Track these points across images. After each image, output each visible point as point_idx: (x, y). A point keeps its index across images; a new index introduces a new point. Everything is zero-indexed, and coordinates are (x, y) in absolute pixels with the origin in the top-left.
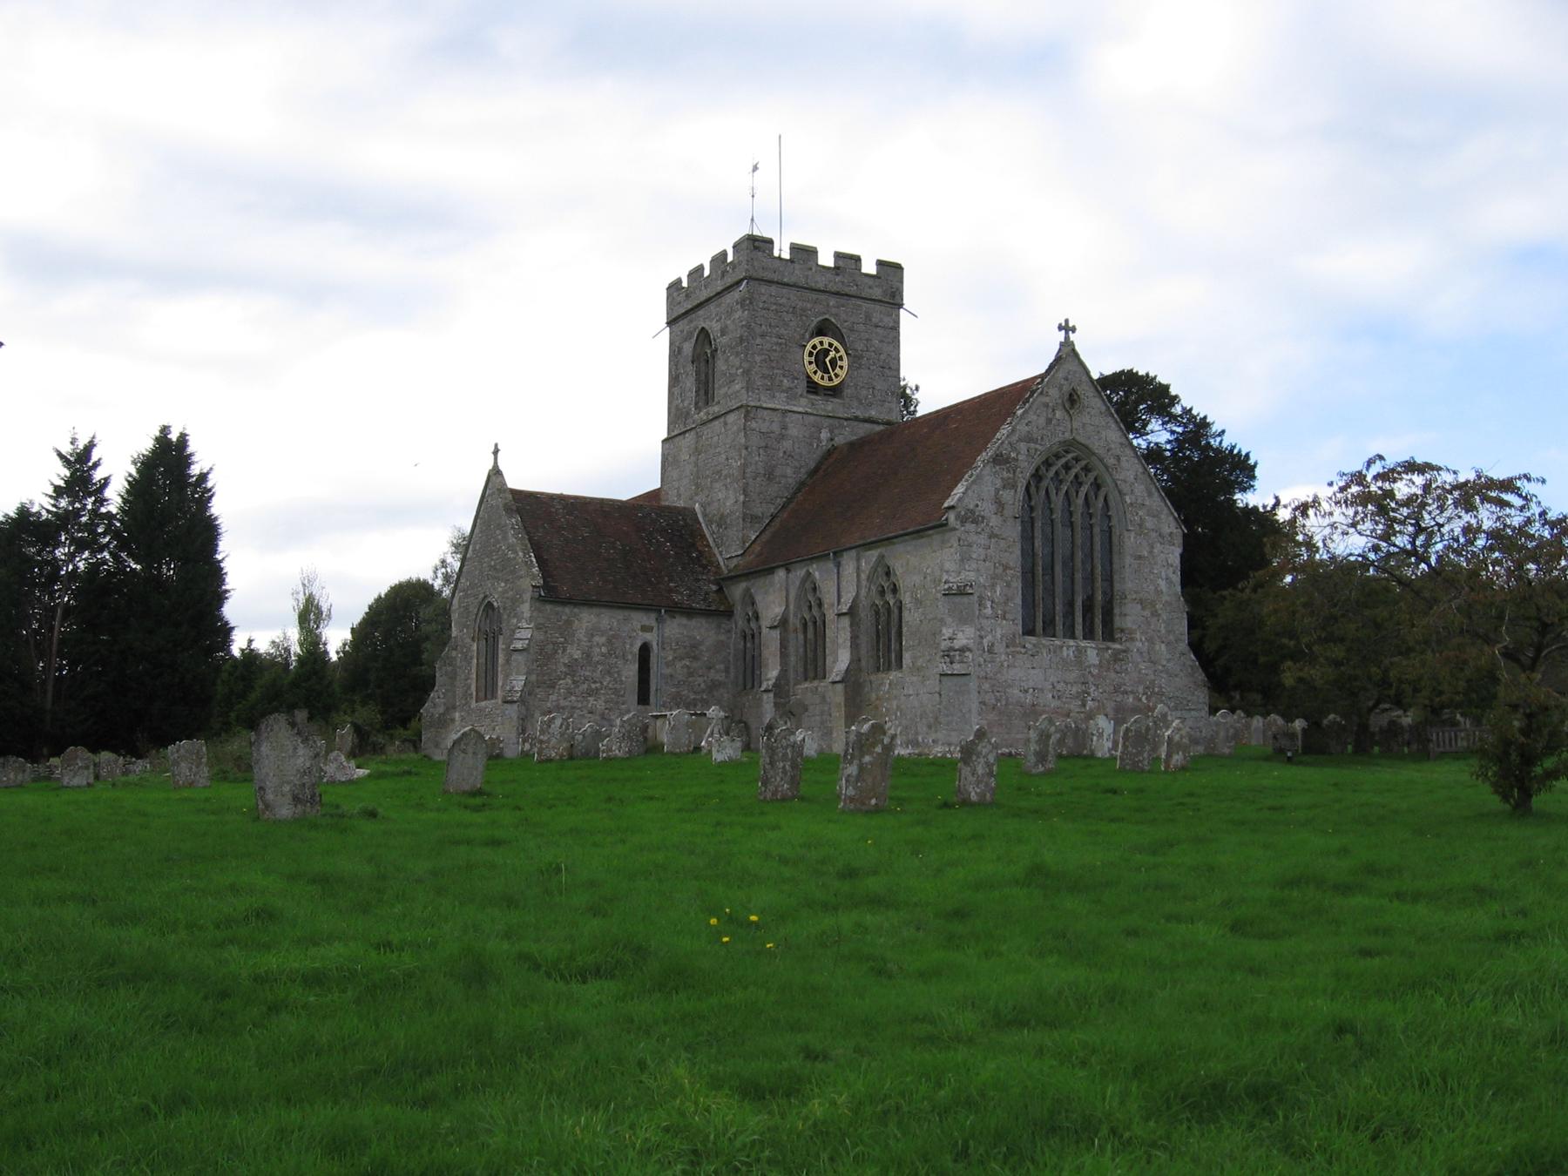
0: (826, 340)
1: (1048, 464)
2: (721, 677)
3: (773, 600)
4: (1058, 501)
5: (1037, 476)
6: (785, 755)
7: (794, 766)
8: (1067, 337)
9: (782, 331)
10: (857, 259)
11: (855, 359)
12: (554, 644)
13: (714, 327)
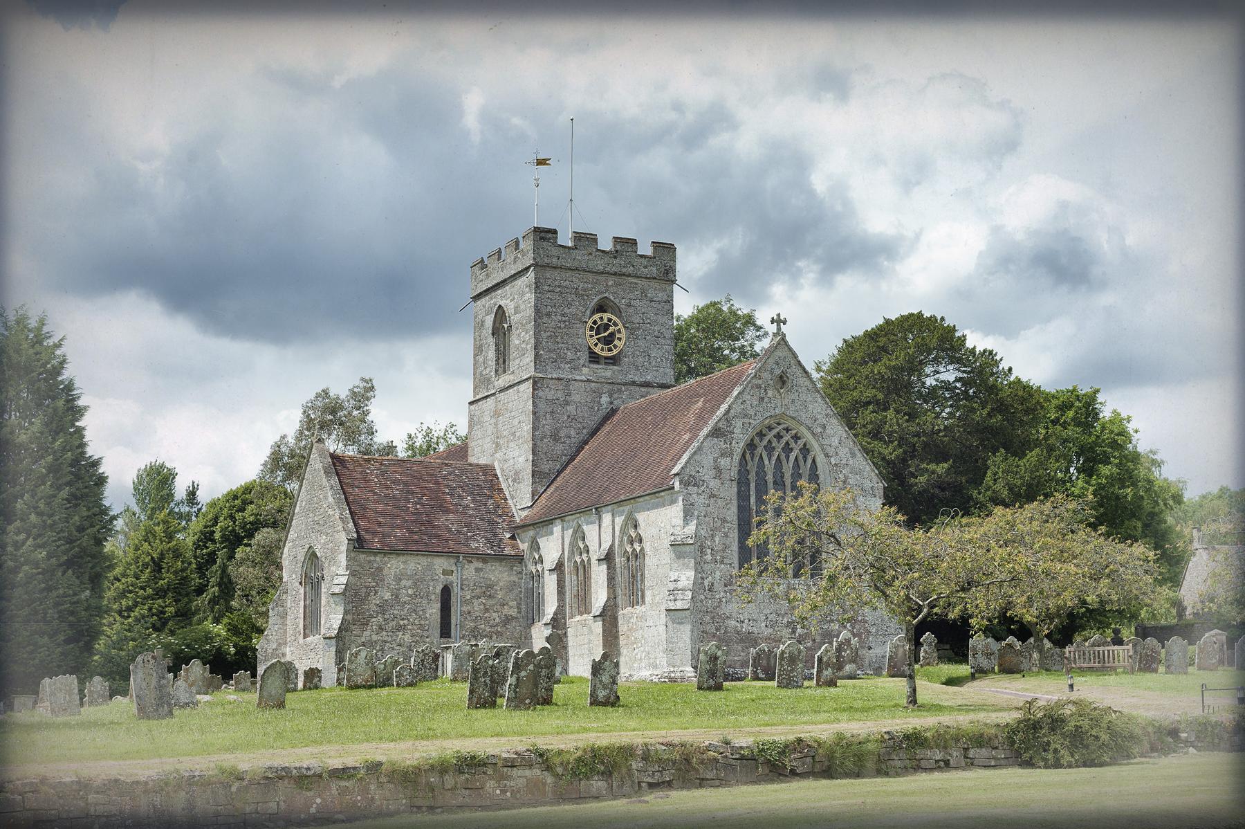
0: (606, 316)
1: (761, 435)
2: (513, 612)
3: (552, 547)
4: (769, 467)
5: (751, 446)
6: (486, 673)
7: (493, 680)
8: (779, 329)
9: (566, 310)
10: (634, 242)
11: (631, 329)
12: (367, 587)
13: (509, 306)
